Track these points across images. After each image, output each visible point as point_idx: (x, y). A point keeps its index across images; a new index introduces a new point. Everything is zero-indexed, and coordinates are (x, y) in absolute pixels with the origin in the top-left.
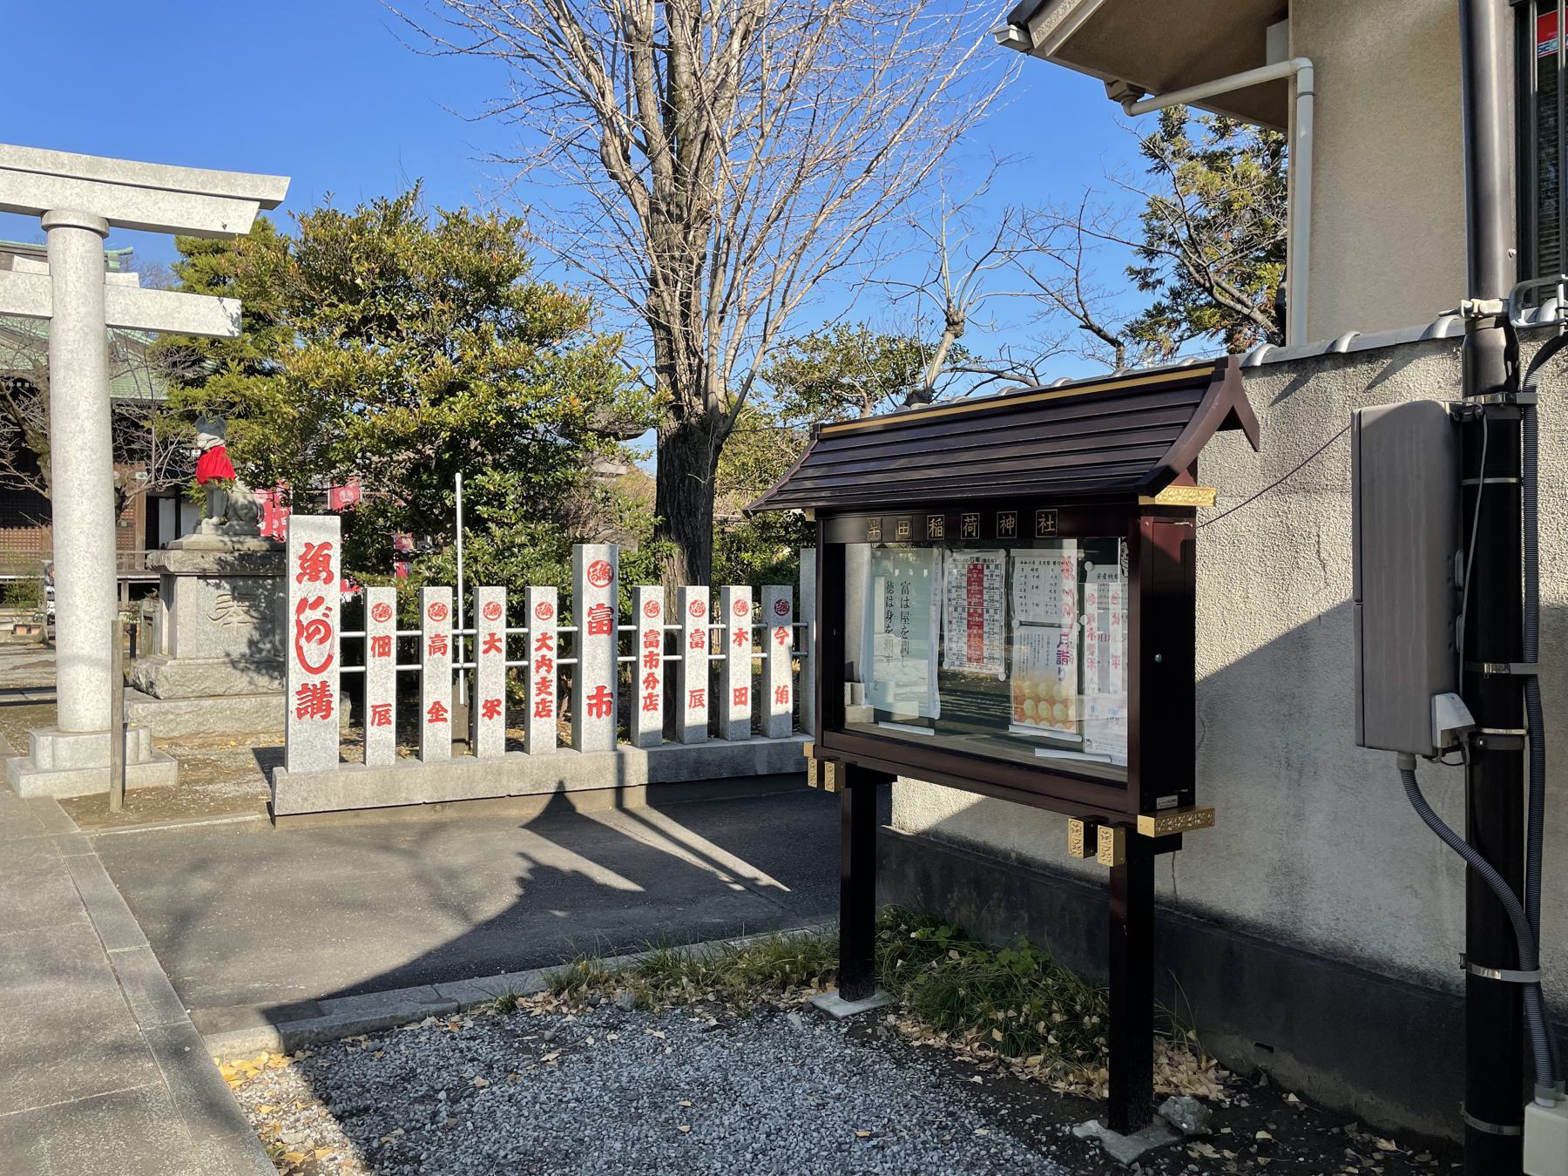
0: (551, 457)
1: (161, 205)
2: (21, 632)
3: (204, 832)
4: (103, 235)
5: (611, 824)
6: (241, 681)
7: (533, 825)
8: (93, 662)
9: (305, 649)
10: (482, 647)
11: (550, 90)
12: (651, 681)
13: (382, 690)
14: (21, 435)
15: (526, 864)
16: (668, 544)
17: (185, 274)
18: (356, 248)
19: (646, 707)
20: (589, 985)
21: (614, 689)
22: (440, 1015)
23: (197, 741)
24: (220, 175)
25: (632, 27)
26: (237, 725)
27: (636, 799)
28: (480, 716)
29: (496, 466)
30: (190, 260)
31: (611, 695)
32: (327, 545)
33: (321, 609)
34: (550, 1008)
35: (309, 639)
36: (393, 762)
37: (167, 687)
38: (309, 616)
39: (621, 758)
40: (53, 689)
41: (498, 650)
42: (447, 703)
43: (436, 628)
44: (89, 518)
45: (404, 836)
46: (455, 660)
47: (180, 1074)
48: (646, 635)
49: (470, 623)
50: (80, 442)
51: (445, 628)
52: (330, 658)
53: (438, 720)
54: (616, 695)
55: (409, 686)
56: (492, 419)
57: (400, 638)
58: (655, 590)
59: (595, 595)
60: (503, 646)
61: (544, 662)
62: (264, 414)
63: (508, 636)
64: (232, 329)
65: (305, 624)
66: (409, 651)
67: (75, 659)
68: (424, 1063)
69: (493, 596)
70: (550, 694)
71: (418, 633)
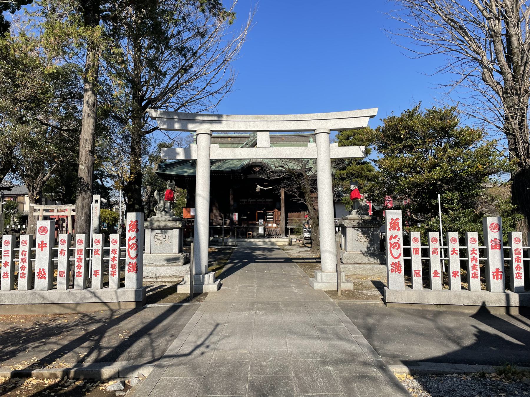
0: (470, 186)
1: (343, 123)
2: (298, 242)
3: (366, 305)
4: (329, 133)
5: (506, 320)
6: (365, 259)
7: (475, 316)
8: (330, 252)
9: (392, 251)
10: (450, 253)
11: (460, 59)
12: (518, 267)
13: (417, 265)
14: (300, 188)
15: (475, 329)
16: (519, 215)
17: (340, 138)
18: (401, 126)
19: (517, 277)
20: (512, 374)
21: (503, 270)
22: (459, 374)
23: (354, 277)
24: (359, 111)
25: (493, 32)
26: (366, 273)
27: (515, 312)
28: (451, 276)
29: (450, 190)
30: (341, 133)
31: (502, 272)
32: (398, 219)
33: (397, 238)
34: (498, 379)
35: (394, 248)
36: (422, 289)
37: (345, 260)
38: (393, 241)
39: (508, 297)
40: (320, 258)
41: (457, 254)
42: (439, 271)
43: (434, 245)
44: (328, 212)
45: (428, 314)
46: (441, 256)
47: (385, 374)
48: (515, 250)
49: (445, 244)
50: (325, 191)
51: (437, 246)
52: (400, 254)
53: (436, 276)
54: (504, 272)
55: (426, 265)
56: (449, 175)
57: (422, 249)
58: (518, 233)
59: (493, 235)
60: (458, 252)
61: (474, 259)
62: (363, 176)
63: (460, 249)
64: (363, 155)
65: (392, 243)
66: (425, 253)
67: (325, 251)
68: (457, 387)
69: (454, 235)
70: (477, 270)
71: (428, 247)
